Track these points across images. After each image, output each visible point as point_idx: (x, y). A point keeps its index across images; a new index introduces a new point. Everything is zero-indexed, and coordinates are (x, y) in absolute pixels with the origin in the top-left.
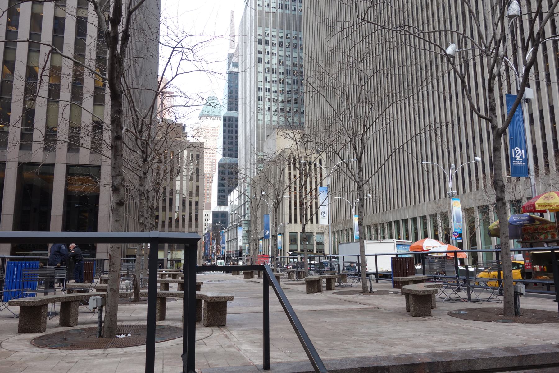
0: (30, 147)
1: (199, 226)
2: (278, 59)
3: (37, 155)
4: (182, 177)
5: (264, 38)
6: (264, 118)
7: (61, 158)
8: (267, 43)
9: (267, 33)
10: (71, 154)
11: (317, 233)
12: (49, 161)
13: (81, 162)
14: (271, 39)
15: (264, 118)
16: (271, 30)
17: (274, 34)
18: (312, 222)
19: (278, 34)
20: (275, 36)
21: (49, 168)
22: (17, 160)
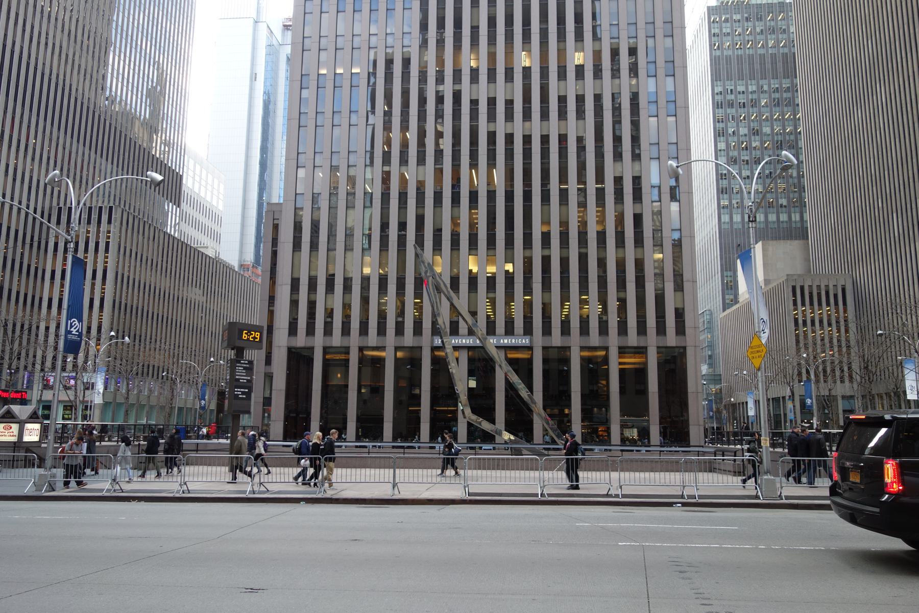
0: (588, 334)
1: (687, 286)
2: (749, 127)
3: (556, 339)
4: (427, 284)
5: (725, 98)
6: (731, 218)
7: (575, 341)
8: (731, 105)
9: (729, 88)
10: (660, 338)
11: (843, 397)
12: (642, 345)
13: (630, 344)
14: (736, 97)
15: (731, 218)
16: (735, 83)
17: (741, 88)
18: (842, 381)
19: (747, 88)
20: (743, 92)
21: (346, 350)
22: (286, 344)
